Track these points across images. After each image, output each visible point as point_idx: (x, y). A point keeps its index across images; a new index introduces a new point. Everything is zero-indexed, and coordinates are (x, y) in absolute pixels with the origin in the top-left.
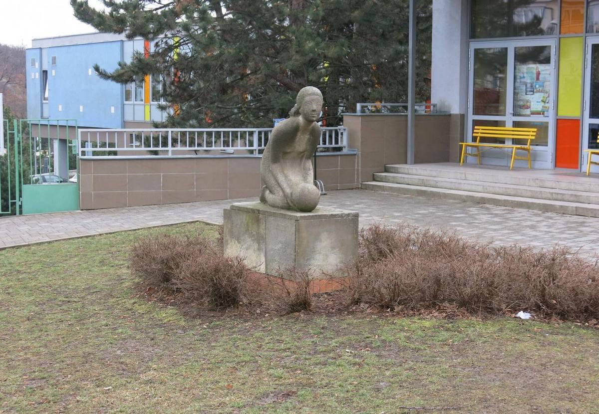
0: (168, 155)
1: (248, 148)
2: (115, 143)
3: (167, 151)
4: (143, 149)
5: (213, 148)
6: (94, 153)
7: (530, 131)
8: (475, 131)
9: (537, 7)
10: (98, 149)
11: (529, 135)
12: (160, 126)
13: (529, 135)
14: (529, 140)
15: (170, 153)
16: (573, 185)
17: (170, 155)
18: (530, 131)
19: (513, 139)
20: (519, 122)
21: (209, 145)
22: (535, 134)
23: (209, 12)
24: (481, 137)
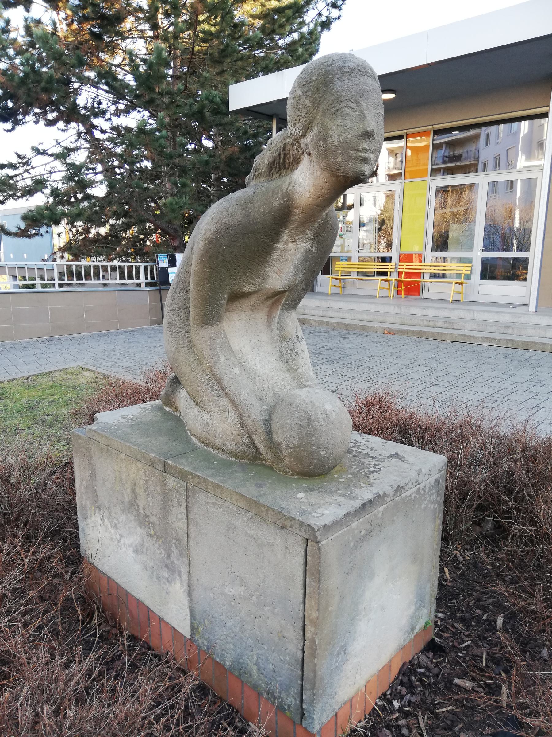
0: (420, 278)
1: (135, 281)
2: (457, 274)
3: (54, 285)
4: (75, 281)
5: (93, 281)
6: (43, 286)
7: (463, 267)
8: (470, 269)
9: (480, 311)
10: (46, 282)
11: (462, 270)
12: (500, 271)
13: (462, 270)
14: (463, 275)
15: (57, 286)
16: (321, 312)
17: (39, 289)
18: (463, 267)
19: (358, 272)
20: (465, 258)
21: (70, 278)
22: (336, 266)
23: (481, 613)
24: (406, 273)
